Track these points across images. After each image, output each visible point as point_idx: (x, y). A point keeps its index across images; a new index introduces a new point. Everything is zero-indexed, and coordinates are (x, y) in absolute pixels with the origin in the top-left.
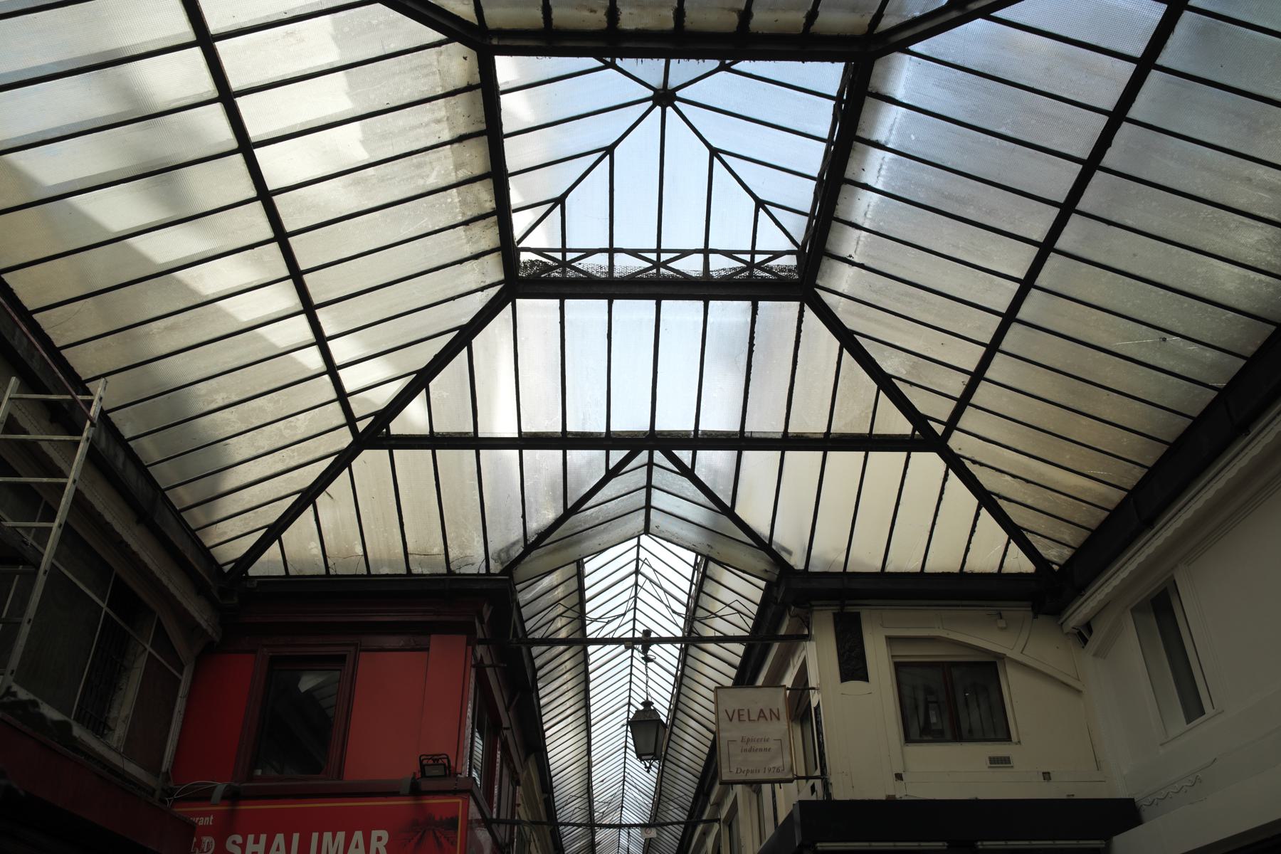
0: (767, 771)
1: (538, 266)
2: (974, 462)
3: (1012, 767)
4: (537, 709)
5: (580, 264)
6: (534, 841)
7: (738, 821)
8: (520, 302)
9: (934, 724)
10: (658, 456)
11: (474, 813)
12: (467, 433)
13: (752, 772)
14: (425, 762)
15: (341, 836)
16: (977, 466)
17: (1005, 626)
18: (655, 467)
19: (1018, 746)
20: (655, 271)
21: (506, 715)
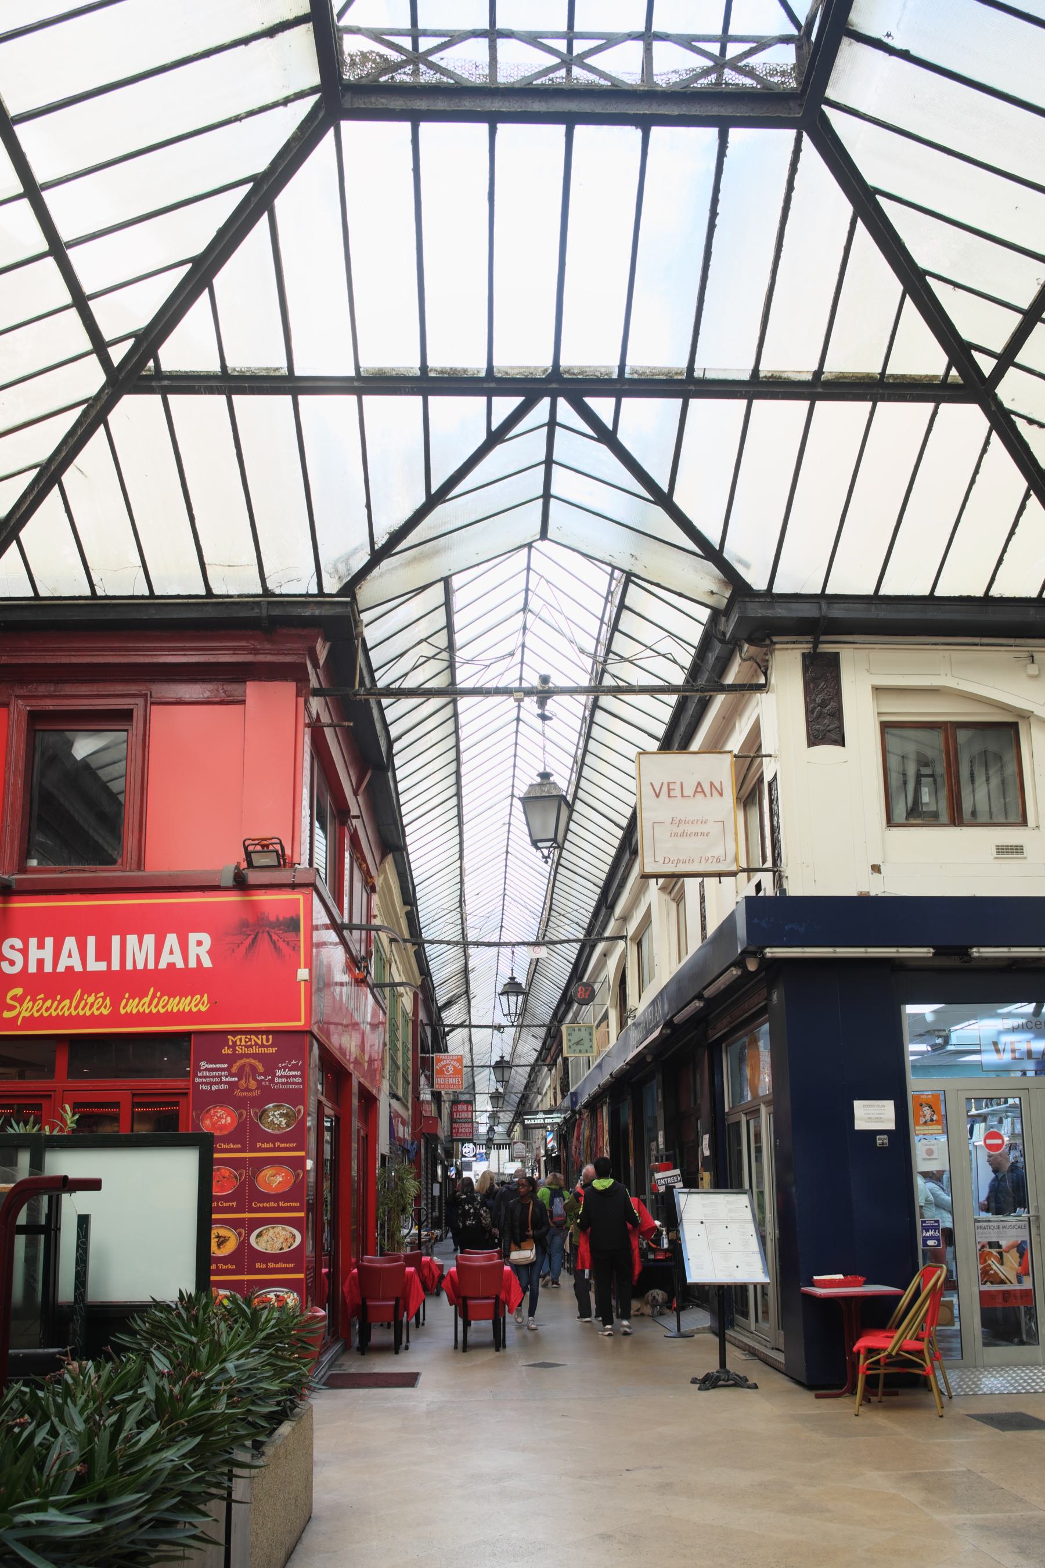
0: (703, 860)
1: (374, 61)
2: (1031, 421)
3: (1025, 858)
4: (394, 795)
5: (442, 59)
6: (396, 962)
7: (651, 940)
8: (347, 126)
9: (927, 804)
10: (565, 411)
11: (320, 917)
12: (277, 369)
13: (684, 862)
14: (250, 849)
15: (149, 939)
16: (1035, 427)
17: (1037, 673)
18: (557, 428)
19: (1036, 831)
20: (563, 72)
21: (355, 800)
